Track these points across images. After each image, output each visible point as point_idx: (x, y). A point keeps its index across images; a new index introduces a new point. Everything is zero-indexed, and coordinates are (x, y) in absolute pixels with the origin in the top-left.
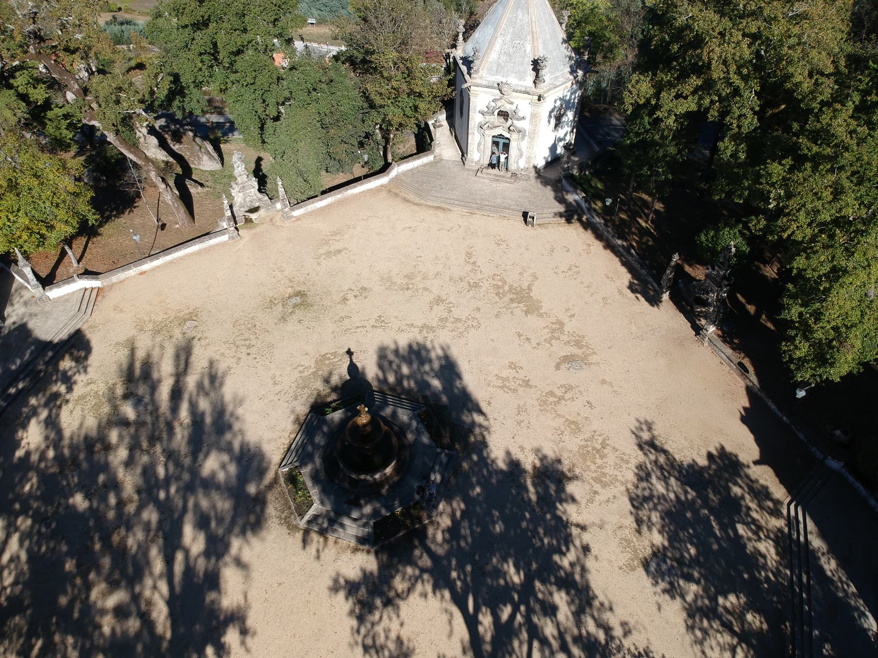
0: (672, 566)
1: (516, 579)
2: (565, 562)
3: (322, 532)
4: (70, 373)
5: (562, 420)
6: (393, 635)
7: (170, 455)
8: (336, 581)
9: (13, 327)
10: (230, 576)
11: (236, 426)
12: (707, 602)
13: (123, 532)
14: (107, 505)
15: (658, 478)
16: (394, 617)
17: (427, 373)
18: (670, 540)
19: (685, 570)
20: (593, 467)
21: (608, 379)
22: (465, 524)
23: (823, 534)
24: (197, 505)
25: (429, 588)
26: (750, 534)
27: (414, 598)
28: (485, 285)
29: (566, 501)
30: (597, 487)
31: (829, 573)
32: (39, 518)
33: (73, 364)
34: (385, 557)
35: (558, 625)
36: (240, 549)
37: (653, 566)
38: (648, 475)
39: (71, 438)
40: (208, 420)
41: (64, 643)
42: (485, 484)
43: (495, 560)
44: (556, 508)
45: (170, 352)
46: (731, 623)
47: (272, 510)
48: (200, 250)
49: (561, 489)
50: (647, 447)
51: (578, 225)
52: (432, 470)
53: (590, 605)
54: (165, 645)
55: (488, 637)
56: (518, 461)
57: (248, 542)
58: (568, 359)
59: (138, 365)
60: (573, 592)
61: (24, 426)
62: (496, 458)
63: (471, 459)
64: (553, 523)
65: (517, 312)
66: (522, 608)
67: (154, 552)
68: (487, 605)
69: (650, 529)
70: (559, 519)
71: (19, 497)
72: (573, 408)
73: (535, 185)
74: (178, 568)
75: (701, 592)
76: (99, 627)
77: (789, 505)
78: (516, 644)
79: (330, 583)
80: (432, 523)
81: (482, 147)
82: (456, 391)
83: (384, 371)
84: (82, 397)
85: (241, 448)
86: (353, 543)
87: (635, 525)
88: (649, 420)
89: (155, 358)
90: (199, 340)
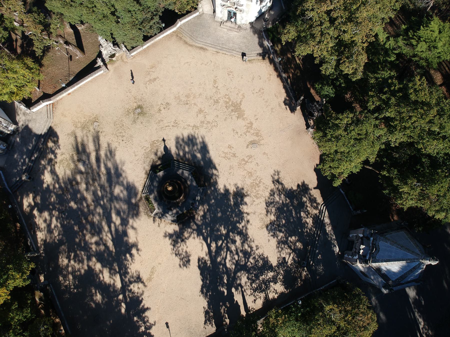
1: (224, 232)
2: (241, 226)
3: (160, 218)
4: (53, 149)
5: (246, 172)
6: (184, 251)
7: (102, 187)
8: (165, 234)
9: (23, 127)
10: (130, 232)
11: (124, 175)
12: (285, 239)
13: (91, 216)
14: (83, 206)
15: (277, 195)
16: (184, 245)
17: (195, 150)
18: (277, 218)
20: (255, 191)
21: (266, 152)
22: (208, 214)
23: (330, 217)
24: (115, 207)
25: (196, 236)
26: (305, 216)
27: (191, 239)
28: (221, 101)
29: (244, 204)
30: (255, 199)
31: (328, 232)
32: (61, 212)
33: (53, 144)
35: (236, 247)
36: (133, 223)
38: (274, 194)
39: (63, 178)
40: (113, 172)
41: (81, 253)
43: (217, 226)
44: (240, 207)
45: (91, 139)
46: (291, 246)
47: (142, 209)
48: (92, 79)
49: (242, 200)
50: (275, 182)
51: (267, 61)
52: (197, 195)
53: (247, 240)
54: (114, 254)
55: (214, 251)
57: (134, 220)
58: (253, 143)
59: (80, 145)
61: (43, 174)
64: (238, 212)
65: (234, 117)
66: (225, 241)
67: (104, 223)
69: (271, 214)
70: (241, 211)
71: (50, 203)
72: (251, 166)
73: (249, 32)
74: (113, 229)
76: (91, 248)
77: (322, 205)
78: (222, 252)
79: (164, 234)
80: (197, 214)
81: (223, 13)
82: (207, 159)
83: (178, 150)
84: (61, 161)
85: (127, 184)
86: (170, 222)
87: (266, 213)
88: (279, 171)
89: (86, 142)
90: (101, 132)
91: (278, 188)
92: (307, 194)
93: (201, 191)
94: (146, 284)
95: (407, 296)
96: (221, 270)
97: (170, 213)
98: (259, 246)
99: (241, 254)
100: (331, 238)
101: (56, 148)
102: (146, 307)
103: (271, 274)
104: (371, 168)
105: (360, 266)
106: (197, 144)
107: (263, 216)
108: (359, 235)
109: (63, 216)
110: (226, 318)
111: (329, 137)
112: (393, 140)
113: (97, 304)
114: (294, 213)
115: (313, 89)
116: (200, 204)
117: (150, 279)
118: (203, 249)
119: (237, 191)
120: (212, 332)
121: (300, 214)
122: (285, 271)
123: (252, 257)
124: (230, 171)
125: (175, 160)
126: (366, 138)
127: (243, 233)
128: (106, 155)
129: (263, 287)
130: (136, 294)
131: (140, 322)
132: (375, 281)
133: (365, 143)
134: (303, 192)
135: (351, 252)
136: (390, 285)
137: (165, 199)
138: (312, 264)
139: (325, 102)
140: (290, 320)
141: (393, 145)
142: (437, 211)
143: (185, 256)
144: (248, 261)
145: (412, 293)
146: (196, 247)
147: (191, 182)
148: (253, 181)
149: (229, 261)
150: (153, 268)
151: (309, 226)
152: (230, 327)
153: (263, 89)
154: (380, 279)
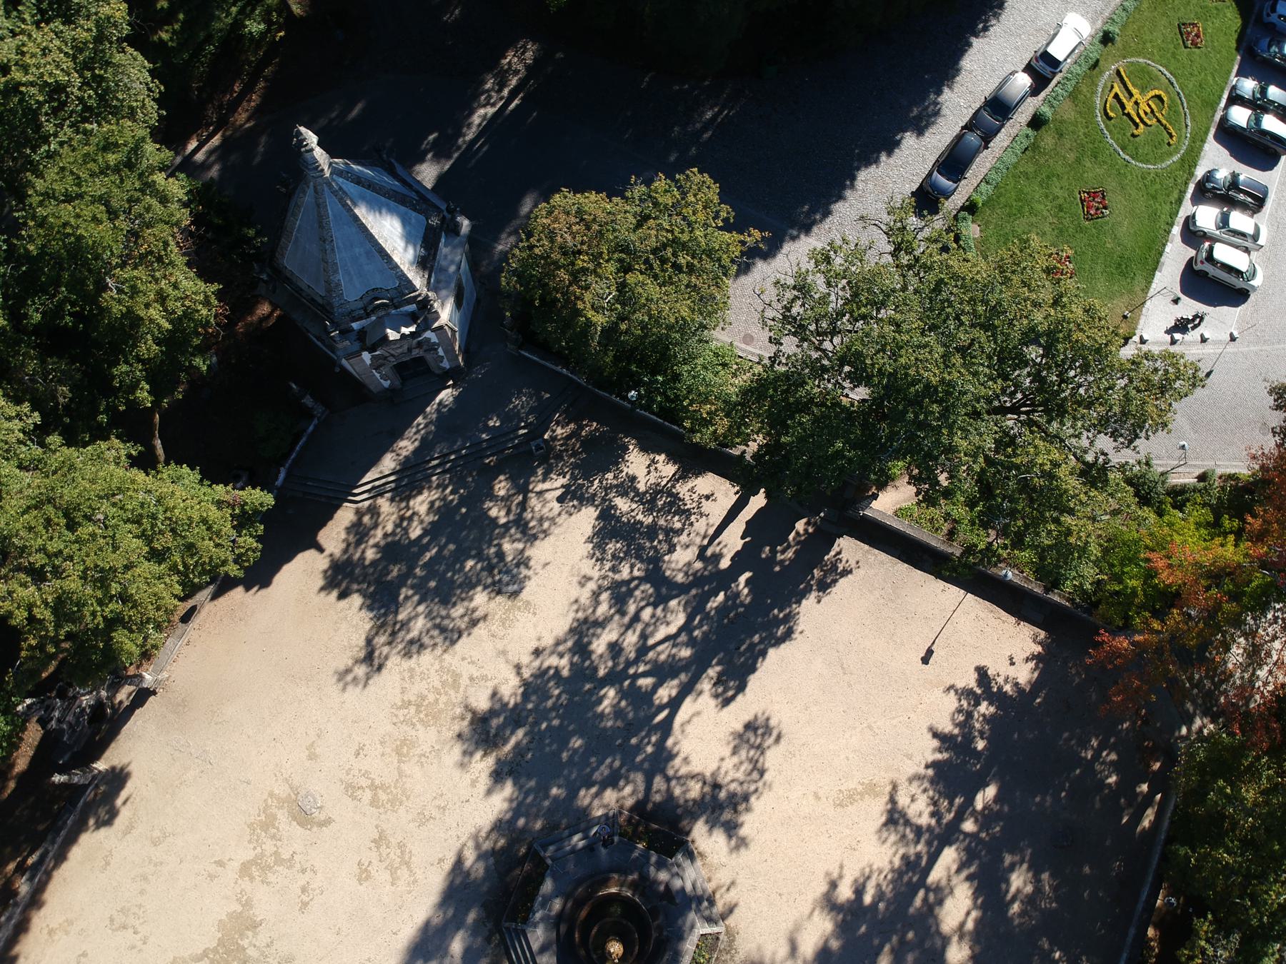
0: (500, 573)
2: (564, 662)
3: (712, 902)
6: (735, 759)
8: (737, 848)
12: (513, 531)
15: (408, 631)
16: (723, 771)
18: (473, 587)
19: (495, 560)
20: (443, 699)
23: (374, 460)
25: (677, 762)
26: (415, 524)
27: (696, 767)
29: (501, 699)
30: (464, 681)
31: (417, 444)
34: (685, 823)
37: (511, 588)
38: (412, 642)
42: (543, 790)
43: (610, 724)
44: (516, 705)
49: (492, 713)
50: (376, 662)
52: (574, 851)
53: (586, 620)
55: (675, 682)
56: (491, 775)
58: (303, 817)
60: (586, 640)
62: (505, 800)
63: (527, 823)
64: (534, 698)
66: (631, 671)
72: (379, 766)
78: (663, 657)
79: (743, 850)
80: (621, 807)
82: (450, 912)
86: (699, 863)
87: (481, 624)
91: (390, 643)
92: (350, 558)
93: (551, 848)
94: (889, 788)
95: (441, 180)
96: (705, 628)
97: (677, 883)
98: (575, 579)
99: (632, 608)
100: (426, 426)
102: (936, 743)
103: (622, 504)
104: (158, 443)
105: (446, 313)
107: (494, 624)
108: (368, 362)
110: (798, 533)
111: (115, 606)
112: (16, 425)
113: (1036, 869)
114: (428, 555)
115: (12, 766)
116: (591, 823)
117: (871, 789)
118: (693, 715)
119: (478, 745)
120: (852, 540)
121: (420, 538)
122: (588, 476)
123: (617, 577)
124: (435, 813)
126: (50, 501)
127: (575, 644)
129: (662, 499)
130: (931, 793)
131: (977, 725)
132: (458, 258)
133: (68, 494)
134: (352, 571)
135: (429, 357)
136: (443, 219)
137: (654, 935)
138: (523, 428)
139: (28, 701)
140: (690, 391)
141: (37, 417)
142: (164, 200)
143: (746, 746)
144: (633, 579)
145: (427, 173)
146: (703, 737)
147: (552, 897)
148: (419, 726)
149: (668, 624)
150: (841, 805)
151: (435, 495)
152: (810, 512)
153: (112, 920)
154: (444, 249)
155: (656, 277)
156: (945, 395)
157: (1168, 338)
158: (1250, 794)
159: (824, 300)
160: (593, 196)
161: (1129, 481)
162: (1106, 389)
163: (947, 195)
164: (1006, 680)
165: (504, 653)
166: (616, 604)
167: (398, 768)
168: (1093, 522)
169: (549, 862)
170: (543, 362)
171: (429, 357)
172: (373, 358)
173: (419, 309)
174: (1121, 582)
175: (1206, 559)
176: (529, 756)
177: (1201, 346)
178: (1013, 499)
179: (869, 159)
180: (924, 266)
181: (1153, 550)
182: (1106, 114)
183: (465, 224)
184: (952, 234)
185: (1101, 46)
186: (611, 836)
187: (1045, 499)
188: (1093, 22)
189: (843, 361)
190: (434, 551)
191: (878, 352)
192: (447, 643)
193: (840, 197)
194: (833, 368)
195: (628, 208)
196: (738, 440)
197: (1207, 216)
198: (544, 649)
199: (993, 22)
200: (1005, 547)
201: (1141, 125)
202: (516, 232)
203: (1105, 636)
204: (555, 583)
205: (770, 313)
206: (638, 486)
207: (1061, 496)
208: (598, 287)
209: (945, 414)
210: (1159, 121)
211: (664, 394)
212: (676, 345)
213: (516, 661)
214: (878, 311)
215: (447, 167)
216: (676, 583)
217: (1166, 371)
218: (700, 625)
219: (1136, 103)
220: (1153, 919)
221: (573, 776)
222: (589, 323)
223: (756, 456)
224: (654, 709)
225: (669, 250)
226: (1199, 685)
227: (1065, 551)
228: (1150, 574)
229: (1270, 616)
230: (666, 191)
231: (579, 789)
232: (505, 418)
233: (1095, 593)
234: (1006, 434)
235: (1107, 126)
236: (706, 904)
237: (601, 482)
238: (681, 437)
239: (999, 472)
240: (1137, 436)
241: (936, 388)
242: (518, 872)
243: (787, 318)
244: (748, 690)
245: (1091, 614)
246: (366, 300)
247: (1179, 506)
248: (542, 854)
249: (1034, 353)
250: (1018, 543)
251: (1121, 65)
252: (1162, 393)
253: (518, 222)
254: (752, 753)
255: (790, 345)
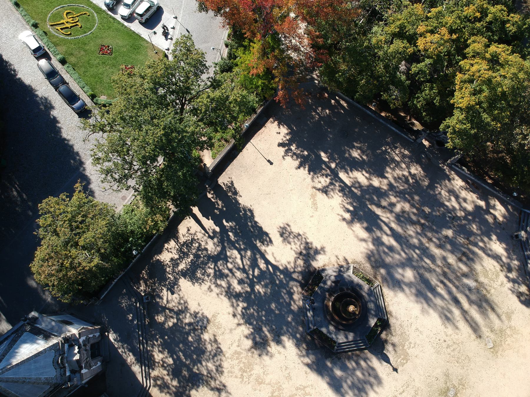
0: (197, 326)
3: (342, 266)
4: (516, 285)
5: (267, 382)
6: (292, 243)
7: (430, 270)
8: (324, 251)
10: (364, 234)
12: (181, 317)
15: (212, 371)
16: (296, 250)
18: (200, 339)
19: (192, 327)
20: (243, 360)
22: (287, 300)
23: (133, 375)
25: (289, 266)
26: (166, 360)
27: (292, 260)
29: (250, 335)
30: (238, 349)
31: (131, 354)
32: (455, 218)
34: (311, 269)
36: (368, 245)
37: (205, 322)
38: (217, 370)
40: (430, 295)
42: (288, 324)
43: (269, 290)
44: (253, 329)
47: (368, 266)
49: (254, 340)
50: (222, 387)
52: (313, 316)
53: (226, 292)
55: (259, 260)
56: (278, 345)
57: (367, 249)
60: (234, 293)
61: (506, 250)
62: (288, 341)
63: (299, 334)
64: (252, 320)
66: (251, 277)
68: (265, 272)
71: (474, 221)
74: (385, 228)
75: (184, 320)
78: (248, 263)
79: (326, 250)
80: (301, 293)
84: (497, 276)
86: (327, 268)
87: (217, 338)
91: (215, 380)
93: (310, 325)
94: (314, 190)
96: (241, 243)
97: (333, 278)
98: (208, 293)
99: (226, 271)
100: (123, 348)
101: (514, 288)
102: (302, 168)
103: (182, 266)
105: (73, 331)
106: (350, 387)
108: (87, 370)
109: (449, 215)
110: (212, 198)
117: (313, 196)
118: (273, 256)
119: (265, 348)
121: (173, 359)
122: (166, 279)
123: (212, 275)
124: (287, 372)
125: (365, 349)
128: (450, 312)
129: (184, 250)
130: (319, 175)
131: (299, 152)
136: (28, 324)
137: (349, 292)
140: (140, 228)
143: (288, 238)
144: (214, 268)
146: (281, 254)
149: (236, 258)
150: (317, 209)
151: (156, 349)
154: (43, 326)
155: (84, 232)
156: (169, 131)
157: (169, 40)
158: (343, 67)
159: (116, 164)
160: (38, 253)
161: (222, 72)
162: (184, 70)
163: (84, 104)
164: (285, 137)
165: (231, 330)
166: (223, 278)
167: (267, 384)
168: (234, 90)
169: (315, 327)
170: (109, 289)
171: (92, 342)
172: (85, 368)
173: (68, 343)
174: (259, 87)
175: (257, 55)
176: (274, 327)
177: (176, 30)
178: (218, 116)
179: (58, 131)
180: (113, 122)
181: (250, 72)
182: (68, 35)
183: (34, 314)
184: (102, 108)
185: (38, 29)
186: (311, 300)
187: (221, 104)
188: (26, 29)
189: (144, 163)
190: (181, 354)
191: (144, 150)
192: (221, 354)
193: (72, 147)
194: (146, 168)
195: (48, 238)
196: (167, 212)
197: (123, 11)
198: (234, 312)
199: (13, 67)
200: (236, 124)
201: (77, 23)
202: (44, 291)
203: (277, 99)
204: (206, 302)
205: (115, 187)
206: (176, 258)
207: (221, 98)
208: (81, 258)
209: (178, 132)
210: (78, 16)
211: (138, 239)
212: (117, 230)
213: (236, 325)
214: (126, 144)
215: (4, 317)
216: (220, 251)
217: (182, 47)
218: (239, 245)
219: (67, 22)
220: (378, 112)
221: (285, 310)
222: (97, 266)
223: (176, 206)
224: (267, 271)
225: (73, 224)
226: (302, 72)
227: (243, 104)
228: (258, 76)
229: (283, 39)
230: (45, 220)
231: (291, 309)
232: (130, 311)
233: (260, 97)
234: (192, 111)
235: (73, 36)
236: (342, 269)
237: (170, 274)
238: (159, 235)
239: (206, 118)
240: (205, 65)
241: (166, 132)
242: (316, 342)
243: (120, 181)
244: (268, 232)
245: (268, 101)
246: (57, 367)
247: (235, 57)
248: (311, 330)
249: (161, 91)
250: (235, 119)
251: (49, 24)
252: (190, 51)
253: (39, 289)
254: (291, 237)
255: (132, 182)
